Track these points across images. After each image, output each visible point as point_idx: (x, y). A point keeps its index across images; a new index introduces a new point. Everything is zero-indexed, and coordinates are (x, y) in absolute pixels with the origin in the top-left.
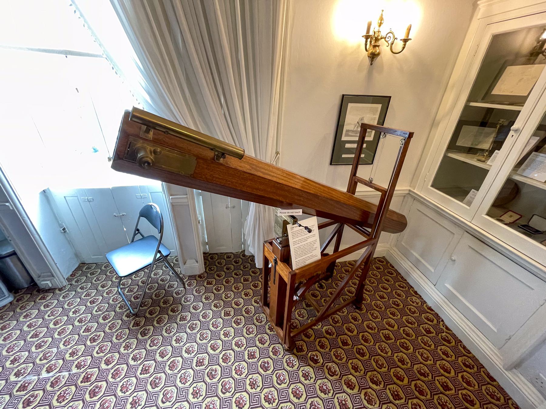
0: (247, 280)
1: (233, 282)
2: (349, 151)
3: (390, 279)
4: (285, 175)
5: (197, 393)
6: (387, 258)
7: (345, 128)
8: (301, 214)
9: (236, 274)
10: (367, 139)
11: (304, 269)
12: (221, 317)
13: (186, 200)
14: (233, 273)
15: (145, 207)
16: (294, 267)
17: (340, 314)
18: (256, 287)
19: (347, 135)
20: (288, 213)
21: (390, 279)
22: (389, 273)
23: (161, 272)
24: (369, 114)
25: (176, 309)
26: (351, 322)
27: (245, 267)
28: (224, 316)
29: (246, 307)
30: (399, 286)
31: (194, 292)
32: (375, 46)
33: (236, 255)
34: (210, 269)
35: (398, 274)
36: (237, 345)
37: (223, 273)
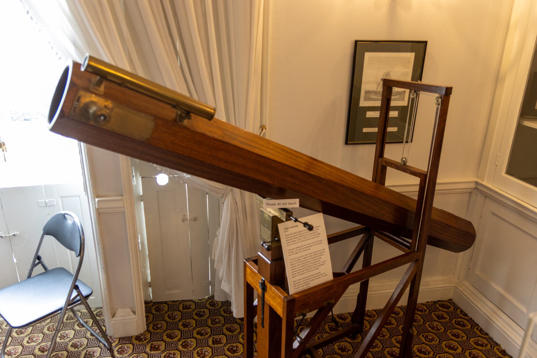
0: (219, 342)
1: (195, 345)
2: (370, 122)
3: (461, 333)
4: (271, 147)
5: (65, 337)
6: (455, 301)
7: (364, 87)
8: (297, 205)
9: (199, 333)
10: (393, 103)
11: (307, 293)
13: (119, 204)
14: (195, 332)
15: (53, 218)
16: (292, 290)
18: (234, 352)
19: (366, 99)
20: (279, 204)
21: (461, 333)
22: (458, 323)
23: (71, 333)
24: (401, 66)
27: (214, 322)
30: (476, 343)
33: (199, 304)
34: (155, 327)
35: (474, 325)
37: (178, 333)
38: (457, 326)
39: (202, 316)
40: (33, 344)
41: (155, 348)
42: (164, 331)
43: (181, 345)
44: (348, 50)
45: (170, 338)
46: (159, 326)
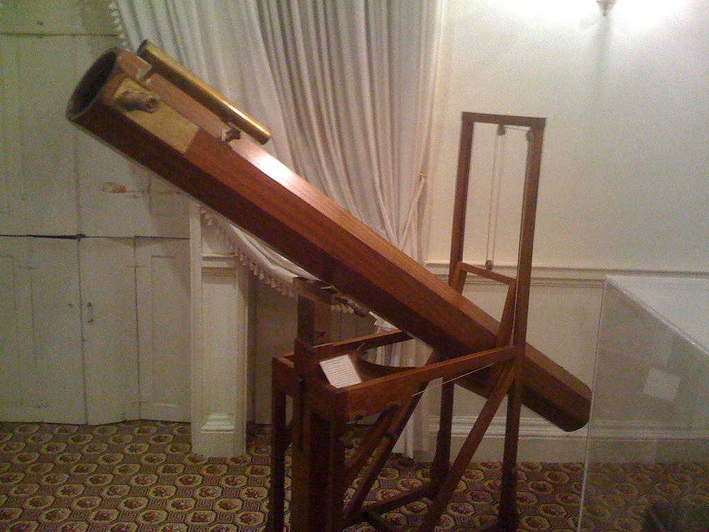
39: (189, 483)
40: (23, 495)
41: (199, 518)
42: (217, 499)
43: (144, 516)
44: (457, 124)
46: (210, 492)
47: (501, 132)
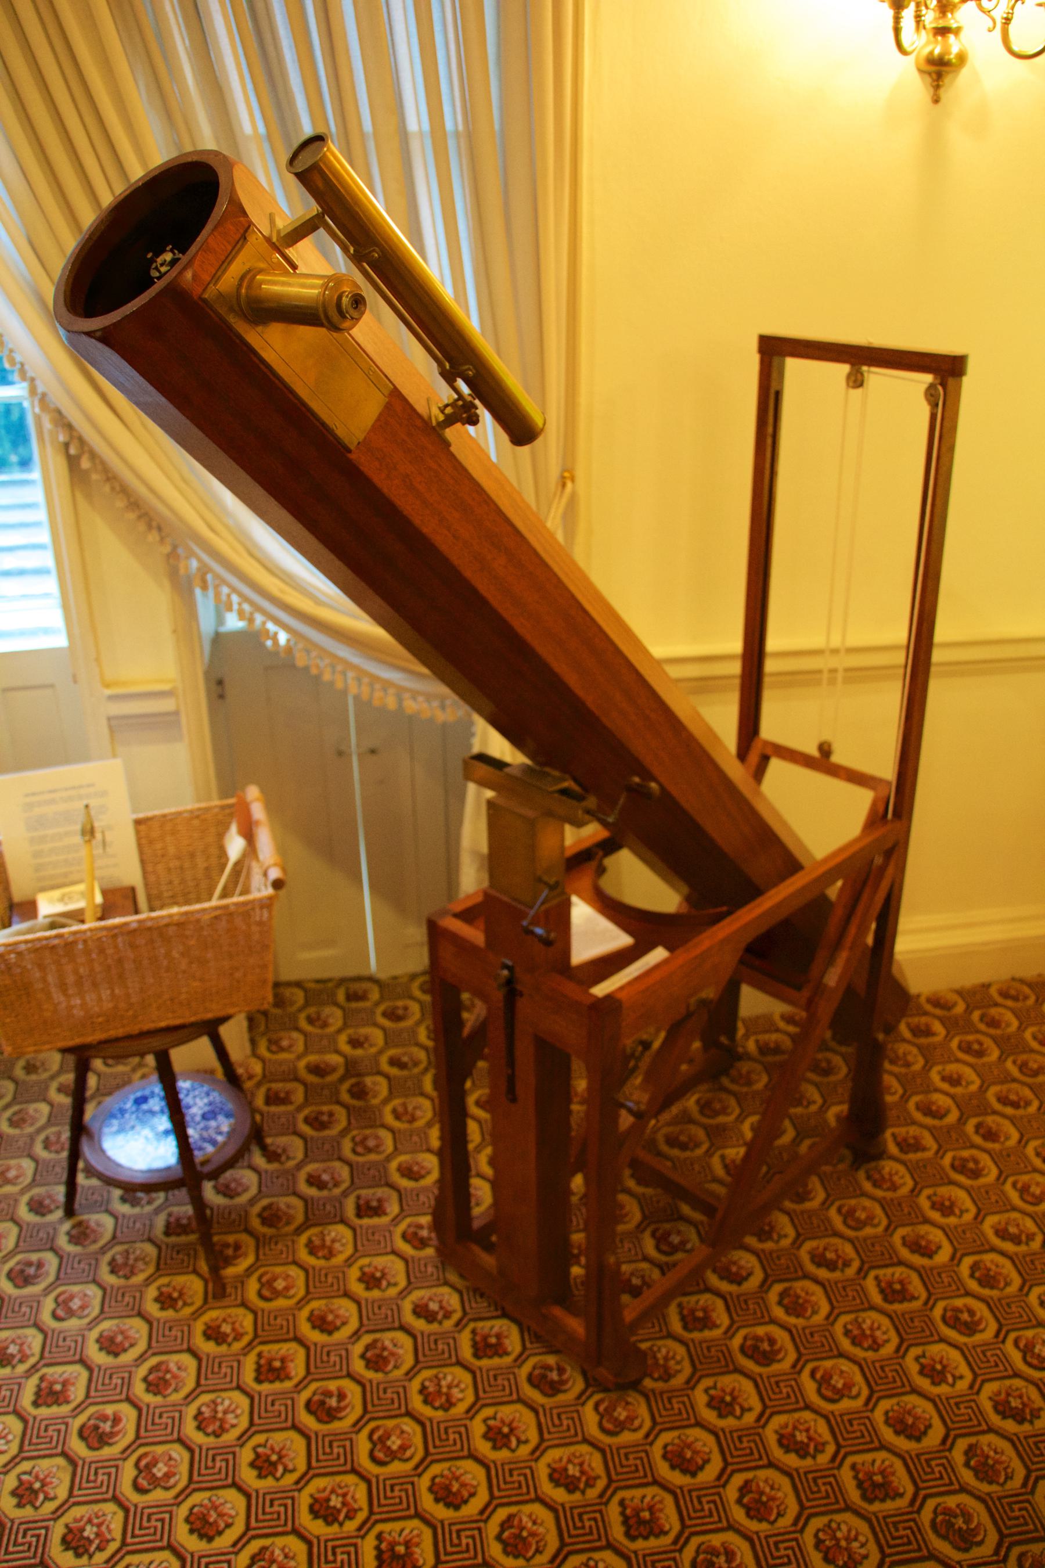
0: (378, 1210)
5: (36, 1493)
12: (239, 1387)
17: (879, 1193)
25: (89, 1532)
26: (915, 1391)
28: (258, 1380)
29: (502, 1514)
31: (104, 1271)
32: (943, 31)
36: (321, 1510)
38: (961, 1055)
43: (363, 1356)
45: (322, 1331)
47: (856, 381)
